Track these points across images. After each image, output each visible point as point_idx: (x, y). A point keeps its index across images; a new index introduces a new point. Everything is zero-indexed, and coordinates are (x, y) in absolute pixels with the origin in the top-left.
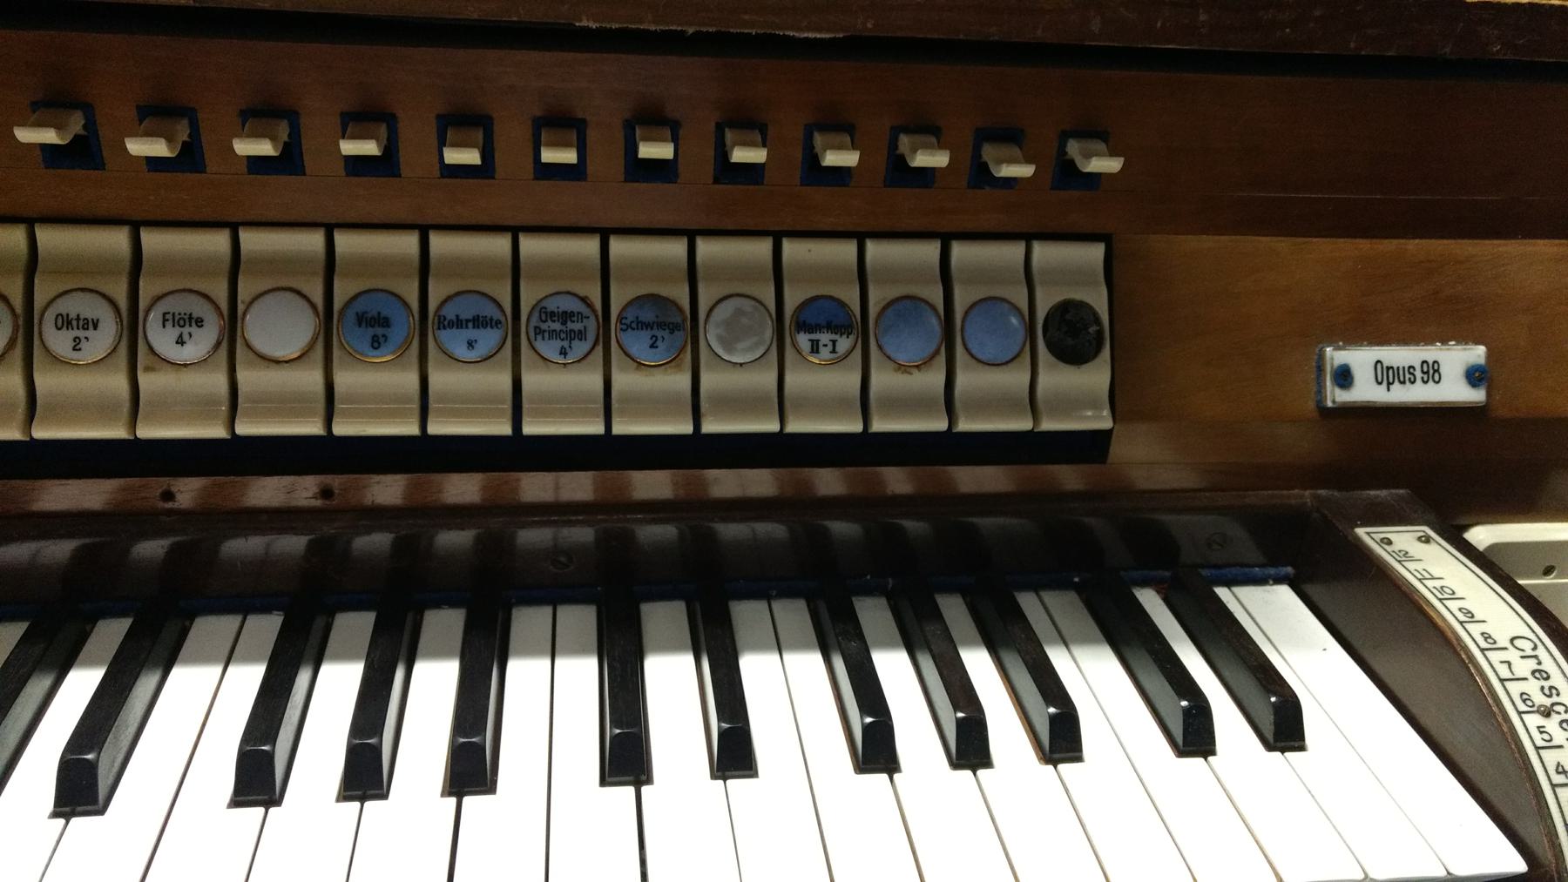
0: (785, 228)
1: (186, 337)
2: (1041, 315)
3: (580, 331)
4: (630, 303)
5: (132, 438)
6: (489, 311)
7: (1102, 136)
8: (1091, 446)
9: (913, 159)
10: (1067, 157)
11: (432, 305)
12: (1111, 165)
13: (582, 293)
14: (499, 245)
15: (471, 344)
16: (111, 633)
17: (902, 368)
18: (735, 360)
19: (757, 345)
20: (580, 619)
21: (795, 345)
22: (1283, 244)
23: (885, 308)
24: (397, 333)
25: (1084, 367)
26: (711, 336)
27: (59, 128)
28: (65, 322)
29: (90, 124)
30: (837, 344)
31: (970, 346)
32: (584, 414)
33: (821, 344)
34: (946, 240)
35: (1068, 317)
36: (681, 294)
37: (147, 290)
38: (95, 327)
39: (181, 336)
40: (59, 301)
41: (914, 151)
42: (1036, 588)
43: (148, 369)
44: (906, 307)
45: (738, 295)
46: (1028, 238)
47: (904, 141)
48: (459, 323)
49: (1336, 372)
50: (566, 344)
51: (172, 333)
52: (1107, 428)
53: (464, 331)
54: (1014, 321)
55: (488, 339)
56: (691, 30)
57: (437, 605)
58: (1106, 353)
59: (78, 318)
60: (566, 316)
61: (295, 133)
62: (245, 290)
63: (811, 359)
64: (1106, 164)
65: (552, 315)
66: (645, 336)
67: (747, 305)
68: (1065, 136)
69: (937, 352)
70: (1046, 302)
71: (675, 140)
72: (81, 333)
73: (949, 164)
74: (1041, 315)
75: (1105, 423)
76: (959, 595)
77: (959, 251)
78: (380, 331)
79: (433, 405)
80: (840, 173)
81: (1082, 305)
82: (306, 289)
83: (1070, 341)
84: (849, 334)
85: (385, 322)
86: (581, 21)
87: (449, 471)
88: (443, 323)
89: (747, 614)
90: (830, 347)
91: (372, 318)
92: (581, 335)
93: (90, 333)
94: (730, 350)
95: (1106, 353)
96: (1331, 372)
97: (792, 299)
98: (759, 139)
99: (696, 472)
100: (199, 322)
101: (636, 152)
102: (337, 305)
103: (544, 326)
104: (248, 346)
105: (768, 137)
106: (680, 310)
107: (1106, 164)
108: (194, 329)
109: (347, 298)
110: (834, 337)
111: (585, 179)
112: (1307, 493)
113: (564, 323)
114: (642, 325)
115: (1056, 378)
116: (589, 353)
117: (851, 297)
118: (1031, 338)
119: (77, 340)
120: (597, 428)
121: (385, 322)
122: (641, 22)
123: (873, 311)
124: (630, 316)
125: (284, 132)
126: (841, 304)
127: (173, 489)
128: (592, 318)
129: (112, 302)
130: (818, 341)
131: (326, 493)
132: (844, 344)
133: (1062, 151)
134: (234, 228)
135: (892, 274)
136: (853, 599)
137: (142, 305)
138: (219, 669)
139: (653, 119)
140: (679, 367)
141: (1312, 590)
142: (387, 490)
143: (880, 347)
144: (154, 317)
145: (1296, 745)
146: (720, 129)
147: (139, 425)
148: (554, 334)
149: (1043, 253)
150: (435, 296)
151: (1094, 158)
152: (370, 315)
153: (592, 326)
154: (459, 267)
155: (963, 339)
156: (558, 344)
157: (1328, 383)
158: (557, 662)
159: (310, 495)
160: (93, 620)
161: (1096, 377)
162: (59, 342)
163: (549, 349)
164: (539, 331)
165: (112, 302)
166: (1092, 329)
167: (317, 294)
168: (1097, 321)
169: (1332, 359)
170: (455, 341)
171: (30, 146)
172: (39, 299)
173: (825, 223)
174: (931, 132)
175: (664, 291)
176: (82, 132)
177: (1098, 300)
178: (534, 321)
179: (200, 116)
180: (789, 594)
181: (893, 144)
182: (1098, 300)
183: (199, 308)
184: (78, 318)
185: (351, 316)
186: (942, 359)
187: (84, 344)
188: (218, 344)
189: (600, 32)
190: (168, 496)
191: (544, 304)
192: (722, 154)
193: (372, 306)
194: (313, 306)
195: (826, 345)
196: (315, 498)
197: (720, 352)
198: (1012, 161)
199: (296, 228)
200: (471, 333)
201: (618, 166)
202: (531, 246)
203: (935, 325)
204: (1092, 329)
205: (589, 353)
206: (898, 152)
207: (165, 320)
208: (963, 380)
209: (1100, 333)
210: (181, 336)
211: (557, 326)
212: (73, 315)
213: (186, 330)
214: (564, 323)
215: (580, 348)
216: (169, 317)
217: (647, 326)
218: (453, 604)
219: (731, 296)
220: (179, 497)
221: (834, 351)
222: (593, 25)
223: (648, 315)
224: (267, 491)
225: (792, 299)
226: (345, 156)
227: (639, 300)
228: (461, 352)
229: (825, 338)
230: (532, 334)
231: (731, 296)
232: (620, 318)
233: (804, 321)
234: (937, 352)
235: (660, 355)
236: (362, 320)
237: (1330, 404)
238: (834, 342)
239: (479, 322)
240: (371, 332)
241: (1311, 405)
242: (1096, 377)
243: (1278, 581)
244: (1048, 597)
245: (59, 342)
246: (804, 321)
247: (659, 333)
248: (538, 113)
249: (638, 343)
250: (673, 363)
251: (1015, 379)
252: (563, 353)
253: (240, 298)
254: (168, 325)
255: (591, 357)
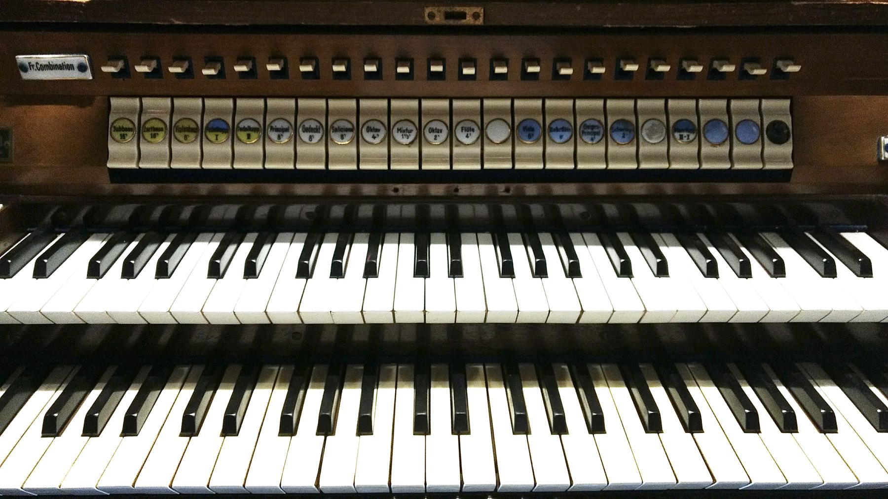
0: (546, 95)
1: (469, 135)
2: (765, 127)
3: (598, 132)
4: (615, 122)
5: (169, 168)
6: (567, 126)
7: (665, 60)
8: (785, 175)
9: (592, 71)
10: (777, 67)
11: (547, 124)
12: (602, 70)
13: (598, 119)
14: (414, 104)
15: (561, 137)
16: (172, 236)
17: (714, 145)
18: (651, 141)
19: (660, 137)
20: (366, 236)
21: (674, 136)
22: (863, 98)
23: (707, 124)
24: (536, 135)
25: (782, 145)
26: (644, 134)
27: (115, 66)
28: (432, 130)
29: (254, 66)
30: (218, 137)
31: (739, 136)
32: (350, 162)
33: (684, 136)
34: (729, 99)
35: (776, 126)
36: (632, 119)
37: (455, 120)
38: (441, 132)
39: (468, 134)
40: (430, 123)
41: (592, 67)
42: (658, 232)
43: (457, 146)
44: (714, 123)
45: (653, 119)
46: (760, 98)
47: (685, 64)
48: (557, 130)
49: (886, 147)
50: (593, 136)
51: (465, 134)
52: (728, 168)
53: (558, 132)
54: (754, 129)
55: (566, 135)
56: (643, 27)
57: (360, 231)
58: (791, 140)
59: (436, 129)
60: (593, 127)
61: (254, 66)
62: (486, 120)
63: (680, 141)
64: (794, 69)
65: (588, 127)
66: (620, 134)
67: (656, 122)
68: (776, 59)
69: (726, 140)
70: (767, 122)
71: (475, 67)
72: (437, 134)
73: (104, 72)
74: (765, 127)
75: (790, 166)
76: (672, 235)
77: (734, 103)
78: (531, 132)
79: (392, 159)
80: (566, 76)
81: (781, 122)
82: (506, 119)
83: (776, 136)
84: (693, 133)
85: (532, 129)
86: (606, 24)
87: (294, 183)
88: (551, 130)
89: (574, 237)
90: (687, 137)
91: (529, 128)
92: (598, 134)
93: (440, 134)
94: (650, 138)
95: (791, 140)
96: (884, 146)
97: (673, 120)
98: (601, 65)
99: (712, 184)
100: (473, 130)
101: (494, 71)
102: (516, 124)
103: (585, 131)
104: (488, 138)
105: (447, 63)
106: (632, 124)
107: (794, 69)
108: (471, 132)
109: (519, 122)
110: (688, 134)
111: (475, 80)
112: (873, 195)
113: (592, 129)
114: (619, 130)
115: (771, 149)
116: (601, 139)
117: (694, 119)
118: (668, 136)
119: (436, 136)
120: (447, 167)
121: (532, 129)
122: (626, 24)
123: (702, 125)
124: (615, 126)
125: (219, 66)
126: (690, 122)
127: (459, 188)
128: (602, 128)
129: (382, 123)
130: (682, 135)
131: (507, 190)
132: (692, 136)
133: (775, 65)
134: (482, 99)
135: (708, 112)
136: (539, 234)
137: (454, 125)
138: (289, 244)
139: (501, 60)
140: (632, 145)
141: (875, 234)
142: (344, 189)
143: (705, 137)
144: (395, 130)
145: (460, 276)
146: (649, 60)
147: (203, 164)
148: (589, 133)
149: (765, 103)
150: (175, 120)
151: (660, 66)
152: (527, 128)
153: (602, 130)
154: (555, 111)
155: (736, 135)
156: (590, 137)
157: (883, 151)
158: (480, 246)
159: (502, 190)
160: (169, 234)
161: (787, 149)
162: (430, 137)
163: (587, 138)
164: (583, 132)
165: (382, 123)
166: (785, 131)
167: (509, 120)
168: (787, 128)
169: (884, 141)
170: (556, 136)
171: (173, 73)
172: (424, 123)
173: (684, 93)
174: (695, 60)
175: (720, 117)
176: (156, 67)
177: (788, 121)
178: (582, 129)
179: (351, 61)
180: (483, 231)
181: (649, 65)
182: (788, 121)
183: (473, 126)
184: (436, 129)
185: (521, 128)
186: (728, 142)
187: (438, 138)
188: (478, 138)
189: (612, 28)
190: (457, 190)
191: (585, 123)
192: (524, 70)
193: (528, 124)
194: (509, 125)
195: (685, 137)
196: (503, 192)
197: (648, 140)
198: (757, 68)
199: (427, 100)
200: (561, 133)
201: (456, 75)
202: (426, 104)
203: (725, 130)
204: (785, 131)
205: (601, 139)
206: (651, 68)
207: (462, 130)
208: (736, 150)
209: (789, 132)
210: (468, 134)
211: (590, 130)
212: (434, 128)
213: (469, 133)
214: (592, 129)
215: (598, 138)
216: (464, 128)
217: (621, 130)
218: (366, 231)
219: (650, 120)
220: (460, 191)
221: (688, 139)
222: (610, 26)
223: (621, 126)
224: (302, 189)
225: (517, 120)
226: (302, 72)
227: (617, 122)
228: (558, 140)
229: (685, 134)
230: (581, 133)
231: (650, 120)
232: (612, 128)
233: (374, 128)
234: (726, 140)
235: (626, 140)
236: (525, 129)
237: (883, 158)
238: (688, 136)
239: (564, 129)
240: (528, 133)
241: (875, 159)
242: (787, 149)
243: (861, 231)
244: (663, 235)
245: (430, 137)
246: (374, 128)
247: (626, 133)
248: (429, 57)
249: (618, 136)
250: (630, 142)
251: (756, 149)
252: (592, 140)
253: (360, 122)
254: (464, 131)
255: (602, 141)
